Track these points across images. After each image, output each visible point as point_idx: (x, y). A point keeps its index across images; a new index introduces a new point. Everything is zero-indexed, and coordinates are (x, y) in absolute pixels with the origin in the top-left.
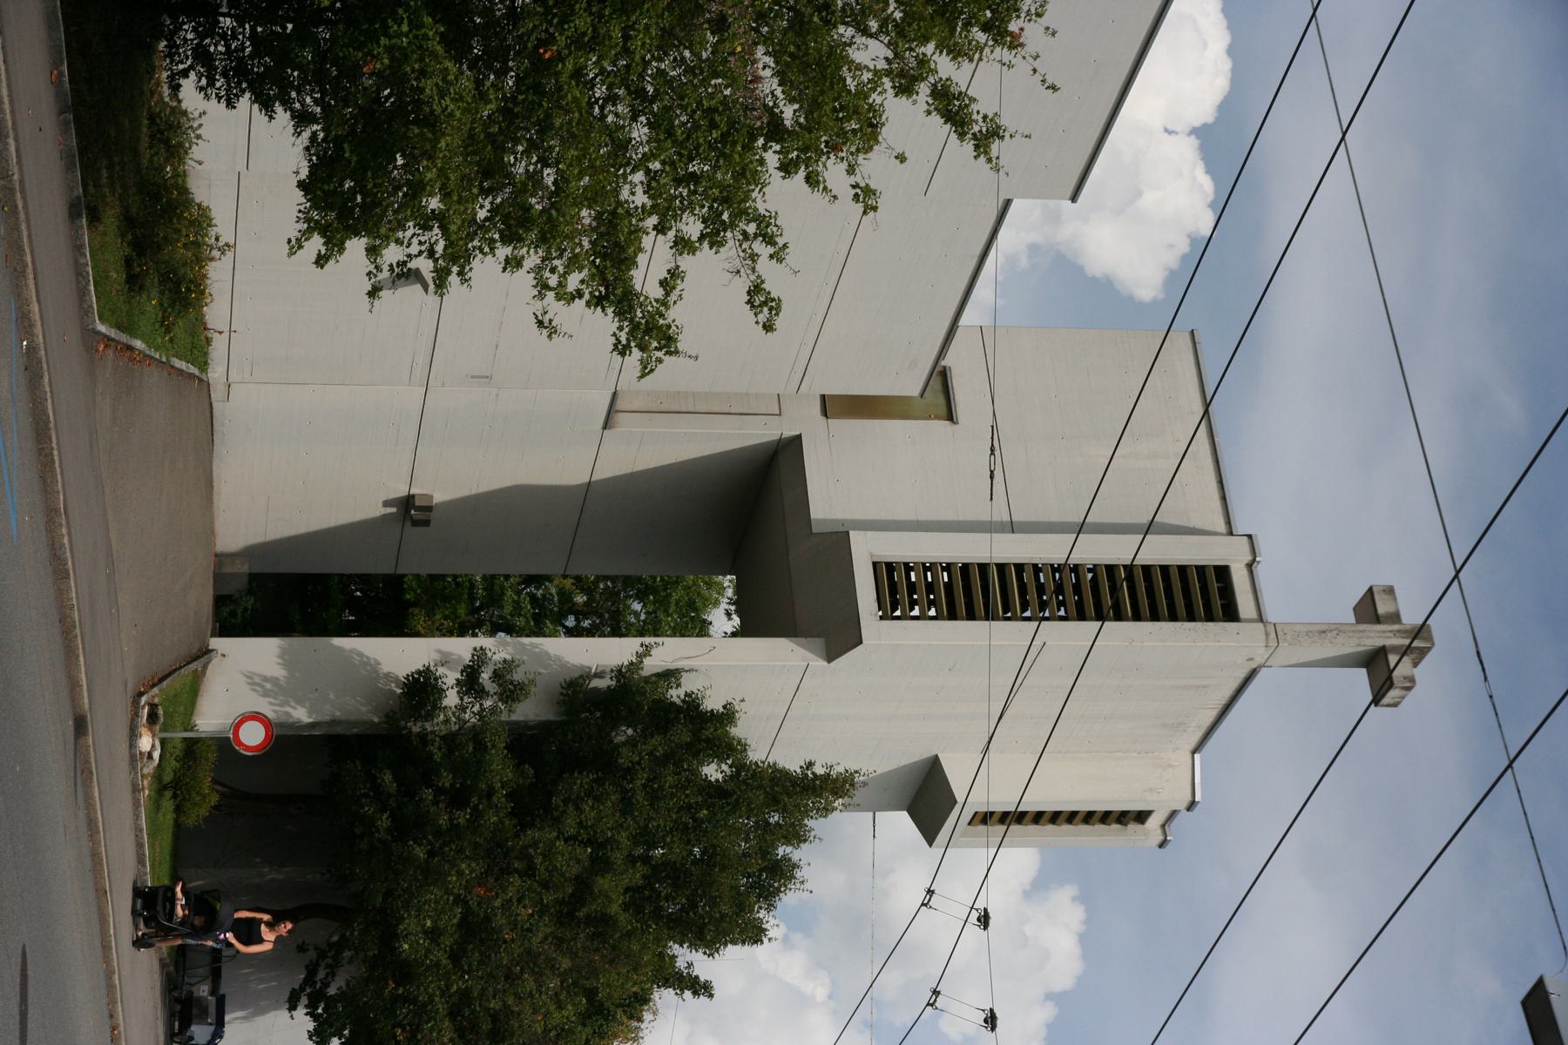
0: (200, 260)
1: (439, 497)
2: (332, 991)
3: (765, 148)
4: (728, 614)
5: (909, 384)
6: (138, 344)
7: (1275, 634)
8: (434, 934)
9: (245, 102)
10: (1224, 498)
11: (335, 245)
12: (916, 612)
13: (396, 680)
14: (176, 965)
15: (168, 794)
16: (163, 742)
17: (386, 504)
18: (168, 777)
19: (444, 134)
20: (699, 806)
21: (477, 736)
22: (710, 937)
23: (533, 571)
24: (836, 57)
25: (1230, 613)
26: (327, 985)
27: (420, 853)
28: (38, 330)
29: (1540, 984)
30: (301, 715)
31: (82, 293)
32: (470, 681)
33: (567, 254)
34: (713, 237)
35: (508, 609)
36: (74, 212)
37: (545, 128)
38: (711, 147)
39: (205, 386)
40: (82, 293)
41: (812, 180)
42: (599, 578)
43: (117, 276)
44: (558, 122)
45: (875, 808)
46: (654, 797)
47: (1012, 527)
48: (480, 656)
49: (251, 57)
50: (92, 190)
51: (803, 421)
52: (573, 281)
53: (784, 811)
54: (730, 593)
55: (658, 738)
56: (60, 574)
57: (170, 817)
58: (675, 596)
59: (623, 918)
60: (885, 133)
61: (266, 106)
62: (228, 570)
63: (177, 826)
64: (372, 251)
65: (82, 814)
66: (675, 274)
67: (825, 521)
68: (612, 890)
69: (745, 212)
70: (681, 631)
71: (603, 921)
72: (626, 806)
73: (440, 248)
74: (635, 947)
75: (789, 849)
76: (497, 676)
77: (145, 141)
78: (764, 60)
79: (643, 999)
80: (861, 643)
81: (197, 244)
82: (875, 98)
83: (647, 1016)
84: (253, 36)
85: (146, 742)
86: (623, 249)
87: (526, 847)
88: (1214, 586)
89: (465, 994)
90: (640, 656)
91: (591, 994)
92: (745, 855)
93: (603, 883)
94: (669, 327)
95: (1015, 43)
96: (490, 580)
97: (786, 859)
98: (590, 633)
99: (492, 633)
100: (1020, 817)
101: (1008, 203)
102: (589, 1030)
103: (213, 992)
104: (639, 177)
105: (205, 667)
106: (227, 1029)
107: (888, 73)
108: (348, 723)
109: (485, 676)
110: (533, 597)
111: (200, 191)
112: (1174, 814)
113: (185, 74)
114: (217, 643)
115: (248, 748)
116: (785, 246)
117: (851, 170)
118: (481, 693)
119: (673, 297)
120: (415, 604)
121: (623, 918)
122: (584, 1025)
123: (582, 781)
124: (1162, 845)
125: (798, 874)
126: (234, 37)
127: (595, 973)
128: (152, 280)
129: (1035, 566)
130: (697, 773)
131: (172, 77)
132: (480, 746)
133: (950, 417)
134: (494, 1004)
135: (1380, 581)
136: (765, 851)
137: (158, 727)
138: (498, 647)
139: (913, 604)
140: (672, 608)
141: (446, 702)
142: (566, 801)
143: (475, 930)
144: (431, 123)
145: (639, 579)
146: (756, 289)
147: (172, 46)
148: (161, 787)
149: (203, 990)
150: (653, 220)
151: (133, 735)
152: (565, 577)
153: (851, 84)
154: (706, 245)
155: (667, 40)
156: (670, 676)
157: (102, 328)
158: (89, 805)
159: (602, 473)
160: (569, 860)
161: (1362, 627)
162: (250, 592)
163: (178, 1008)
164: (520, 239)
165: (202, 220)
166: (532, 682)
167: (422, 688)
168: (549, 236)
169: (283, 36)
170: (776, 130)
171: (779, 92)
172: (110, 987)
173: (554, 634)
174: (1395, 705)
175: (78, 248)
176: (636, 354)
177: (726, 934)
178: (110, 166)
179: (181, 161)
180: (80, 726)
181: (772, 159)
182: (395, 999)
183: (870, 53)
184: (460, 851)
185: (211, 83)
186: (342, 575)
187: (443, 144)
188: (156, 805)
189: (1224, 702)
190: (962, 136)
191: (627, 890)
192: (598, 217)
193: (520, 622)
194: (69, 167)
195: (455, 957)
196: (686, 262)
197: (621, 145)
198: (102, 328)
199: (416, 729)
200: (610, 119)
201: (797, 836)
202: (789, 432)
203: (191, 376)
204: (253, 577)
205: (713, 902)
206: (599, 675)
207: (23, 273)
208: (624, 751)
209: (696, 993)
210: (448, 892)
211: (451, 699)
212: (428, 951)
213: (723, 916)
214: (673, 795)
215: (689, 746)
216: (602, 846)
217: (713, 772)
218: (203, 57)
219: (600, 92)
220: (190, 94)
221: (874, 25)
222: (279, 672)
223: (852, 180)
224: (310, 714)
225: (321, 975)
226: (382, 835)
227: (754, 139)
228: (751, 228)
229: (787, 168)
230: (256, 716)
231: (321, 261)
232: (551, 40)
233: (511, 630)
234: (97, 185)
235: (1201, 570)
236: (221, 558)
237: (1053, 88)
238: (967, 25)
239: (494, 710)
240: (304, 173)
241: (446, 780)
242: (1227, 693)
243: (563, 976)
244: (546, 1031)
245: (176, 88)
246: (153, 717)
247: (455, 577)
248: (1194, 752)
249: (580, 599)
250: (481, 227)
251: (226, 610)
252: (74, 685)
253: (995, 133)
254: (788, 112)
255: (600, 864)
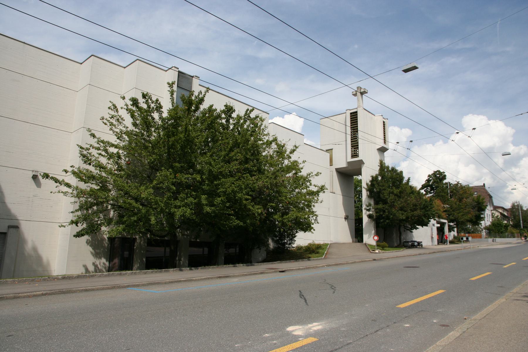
0: (315, 245)
1: (344, 215)
2: (410, 227)
3: (298, 175)
4: (359, 177)
5: (328, 155)
6: (326, 252)
7: (359, 106)
8: (402, 214)
9: (295, 239)
10: (341, 114)
11: (312, 228)
12: (358, 153)
13: (368, 220)
14: (407, 247)
15: (384, 248)
16: (377, 249)
17: (345, 221)
18: (382, 249)
19: (298, 216)
20: (385, 180)
21: (376, 209)
22: (402, 178)
23: (354, 202)
24: (287, 166)
25: (356, 112)
26: (409, 228)
27: (391, 216)
28: (324, 265)
29: (403, 71)
30: (373, 232)
31: (319, 259)
32: (369, 210)
33: (312, 199)
34: (309, 181)
35: (359, 205)
36: (310, 260)
37: (297, 202)
38: (298, 182)
39: (331, 244)
40: (319, 259)
41: (302, 169)
42: (355, 193)
43: (317, 255)
44: (296, 201)
45: (384, 157)
46: (383, 186)
47: (346, 141)
48: (365, 209)
49: (289, 238)
50: (306, 258)
51: (333, 168)
52: (316, 199)
53: (385, 169)
54: (356, 177)
55: (376, 186)
56: (355, 262)
57: (387, 248)
58: (357, 184)
59: (400, 189)
60: (296, 160)
61: (295, 236)
62: (355, 241)
63: (388, 247)
64: (313, 224)
65: (386, 259)
66: (314, 185)
67: (346, 165)
68: (396, 191)
69: (306, 177)
70: (361, 183)
71: (400, 192)
72: (385, 190)
73: (312, 216)
74: (404, 188)
75: (390, 168)
76: (368, 207)
77: (300, 251)
78: (287, 175)
79: (411, 186)
80: (362, 160)
81: (313, 245)
82: (292, 161)
83: (413, 186)
84: (287, 238)
85: (377, 251)
86: (312, 192)
87: (390, 203)
88: (353, 114)
89: (411, 210)
90: (365, 188)
91: (410, 193)
92: (391, 174)
93: (395, 192)
94: (321, 186)
95: (284, 145)
96: (355, 208)
97: (391, 168)
98: (362, 195)
99: (362, 207)
100: (385, 140)
101: (304, 143)
102: (415, 193)
103: (410, 242)
104: (302, 190)
105: (367, 244)
106: (415, 240)
107: (289, 160)
108: (374, 226)
109: (368, 208)
110: (357, 202)
111: (307, 244)
112: (383, 118)
113: (292, 246)
114: (364, 242)
115: (378, 238)
116: (311, 172)
117: (301, 164)
118: (370, 209)
119: (317, 186)
120: (359, 217)
121: (400, 189)
122: (414, 194)
123: (381, 196)
124: (387, 119)
125: (393, 167)
126: (287, 240)
127: (407, 193)
128: (318, 250)
129: (351, 138)
130: (380, 181)
131: (292, 248)
132: (377, 209)
133: (332, 149)
134: (412, 206)
135: (351, 94)
136: (390, 171)
137: (375, 250)
138: (364, 207)
139: (357, 153)
140: (358, 184)
141: (371, 213)
142: (384, 197)
143: (402, 209)
144: (297, 217)
145: (355, 188)
146: (316, 175)
147: (289, 248)
148: (383, 249)
149: (410, 243)
150: (308, 189)
151: (376, 253)
152: (355, 198)
153: (290, 164)
154: (310, 182)
155: (285, 187)
156: (367, 184)
157: (323, 257)
158: (385, 259)
159: (341, 193)
160: (392, 197)
161: (357, 95)
162: (357, 238)
163: (413, 247)
164: (311, 205)
165: (310, 244)
166: (368, 202)
167: (370, 216)
168: (310, 202)
169: (287, 234)
170: (296, 173)
171: (291, 173)
172: (410, 256)
173: (362, 199)
174: (367, 91)
175: (313, 260)
176: (325, 190)
177: (401, 176)
178: (304, 255)
179: (303, 247)
180: (374, 260)
181: (300, 174)
182: (411, 219)
183: (286, 162)
184: (391, 211)
185: (293, 243)
186: (355, 226)
187: (299, 216)
188: (386, 250)
189: (368, 112)
190: (296, 150)
191: (396, 189)
192: (308, 195)
193: (361, 204)
194: (304, 260)
195: (405, 211)
196: (313, 184)
197: (298, 192)
198: (323, 257)
199: (375, 217)
200: (295, 194)
201: (388, 167)
202: (335, 170)
203: (330, 245)
204: (355, 238)
205: (397, 178)
206: (367, 193)
207: (316, 266)
208: (377, 190)
209: (410, 180)
210: (397, 213)
211: (371, 213)
212: (405, 215)
213: (399, 176)
214: (383, 184)
215: (376, 182)
216: (390, 193)
217: (380, 178)
218: (290, 244)
219: (292, 195)
220: (294, 245)
221: (283, 162)
222: (368, 235)
223: (302, 163)
224: (373, 231)
225: (408, 228)
226: (389, 221)
227: (297, 176)
228: (308, 176)
229: (301, 172)
230: (373, 238)
231: (314, 230)
232: (286, 202)
233: (362, 205)
234: (306, 257)
235: (351, 116)
236: (353, 242)
237: (290, 139)
238: (283, 150)
239: (372, 207)
240: (303, 232)
241: (382, 213)
242: (367, 112)
243: (408, 197)
244: (415, 199)
245: (294, 247)
246: (374, 251)
247: (355, 212)
248: (375, 116)
249: (358, 196)
250: (309, 210)
251: (360, 241)
252: (369, 261)
253: (295, 146)
254: (294, 172)
255: (392, 193)
